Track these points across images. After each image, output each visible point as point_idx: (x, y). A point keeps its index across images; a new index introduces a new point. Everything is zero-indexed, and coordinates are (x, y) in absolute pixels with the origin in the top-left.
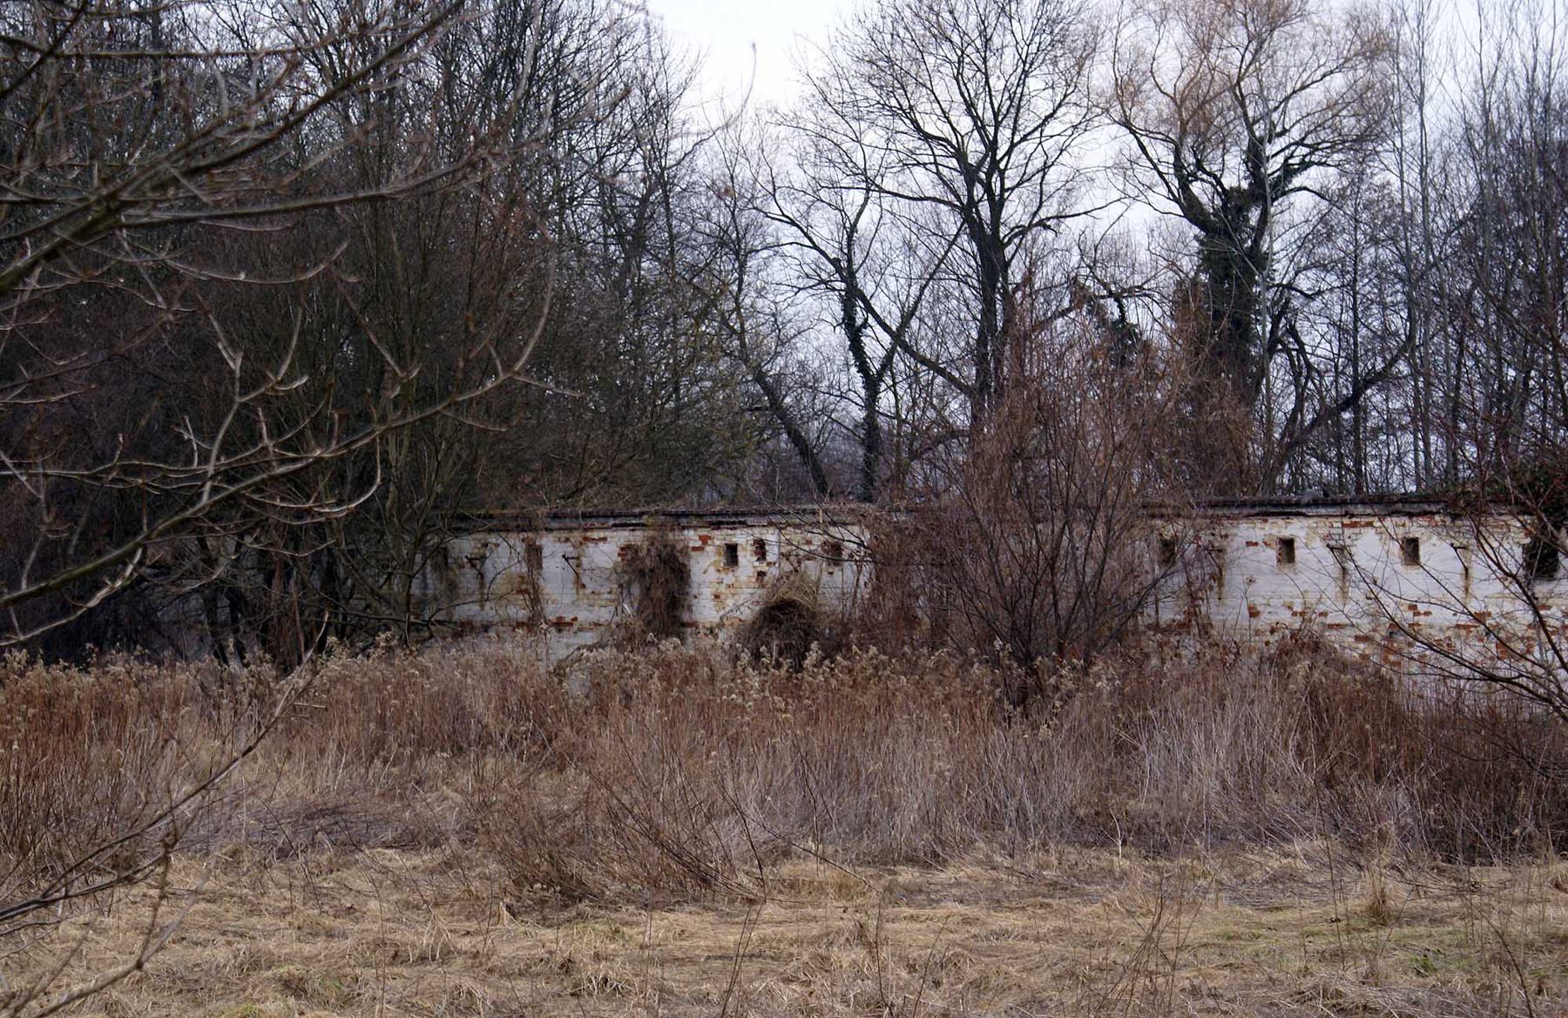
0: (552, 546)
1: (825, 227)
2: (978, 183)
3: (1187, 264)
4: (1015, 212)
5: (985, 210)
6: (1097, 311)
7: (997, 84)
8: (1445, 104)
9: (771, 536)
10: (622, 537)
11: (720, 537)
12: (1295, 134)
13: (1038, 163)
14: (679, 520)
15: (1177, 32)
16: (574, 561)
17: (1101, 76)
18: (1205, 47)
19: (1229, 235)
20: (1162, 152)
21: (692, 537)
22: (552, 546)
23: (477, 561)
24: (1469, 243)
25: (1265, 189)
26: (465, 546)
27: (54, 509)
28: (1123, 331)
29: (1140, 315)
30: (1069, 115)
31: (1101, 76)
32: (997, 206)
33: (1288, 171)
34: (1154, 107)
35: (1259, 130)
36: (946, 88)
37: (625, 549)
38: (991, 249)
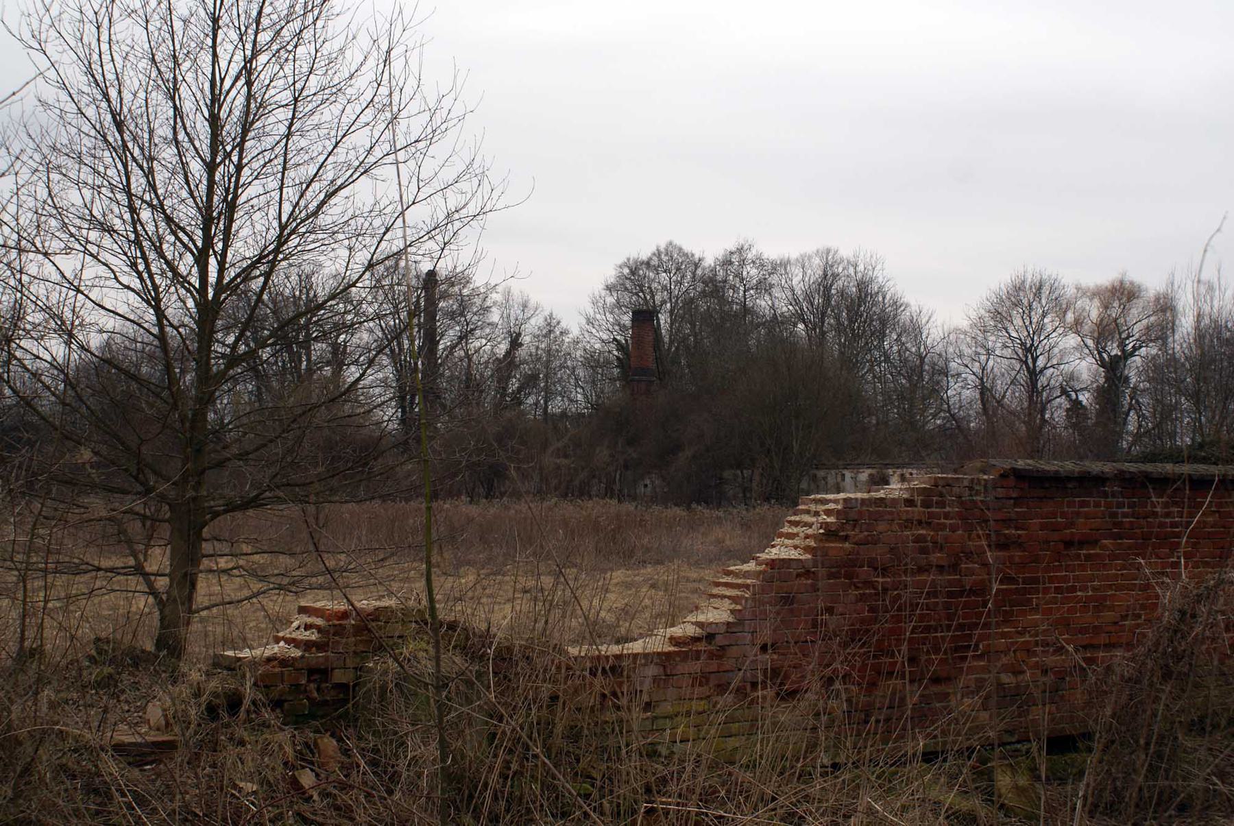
0: (848, 474)
1: (976, 367)
2: (1029, 351)
3: (1102, 381)
4: (1041, 362)
5: (1030, 361)
6: (1069, 396)
7: (1035, 320)
8: (1186, 324)
9: (914, 471)
10: (869, 471)
11: (899, 471)
12: (1137, 336)
13: (1047, 348)
14: (887, 466)
15: (1096, 302)
16: (854, 479)
17: (1070, 317)
18: (1106, 308)
19: (1113, 368)
20: (1090, 342)
21: (890, 471)
22: (848, 474)
23: (825, 478)
24: (498, 370)
25: (1126, 356)
26: (821, 473)
27: (831, 520)
28: (1077, 403)
29: (1084, 398)
30: (1060, 330)
31: (1070, 317)
32: (1035, 360)
33: (1135, 349)
34: (1087, 328)
35: (1124, 336)
36: (1018, 321)
37: (870, 475)
38: (1034, 374)
